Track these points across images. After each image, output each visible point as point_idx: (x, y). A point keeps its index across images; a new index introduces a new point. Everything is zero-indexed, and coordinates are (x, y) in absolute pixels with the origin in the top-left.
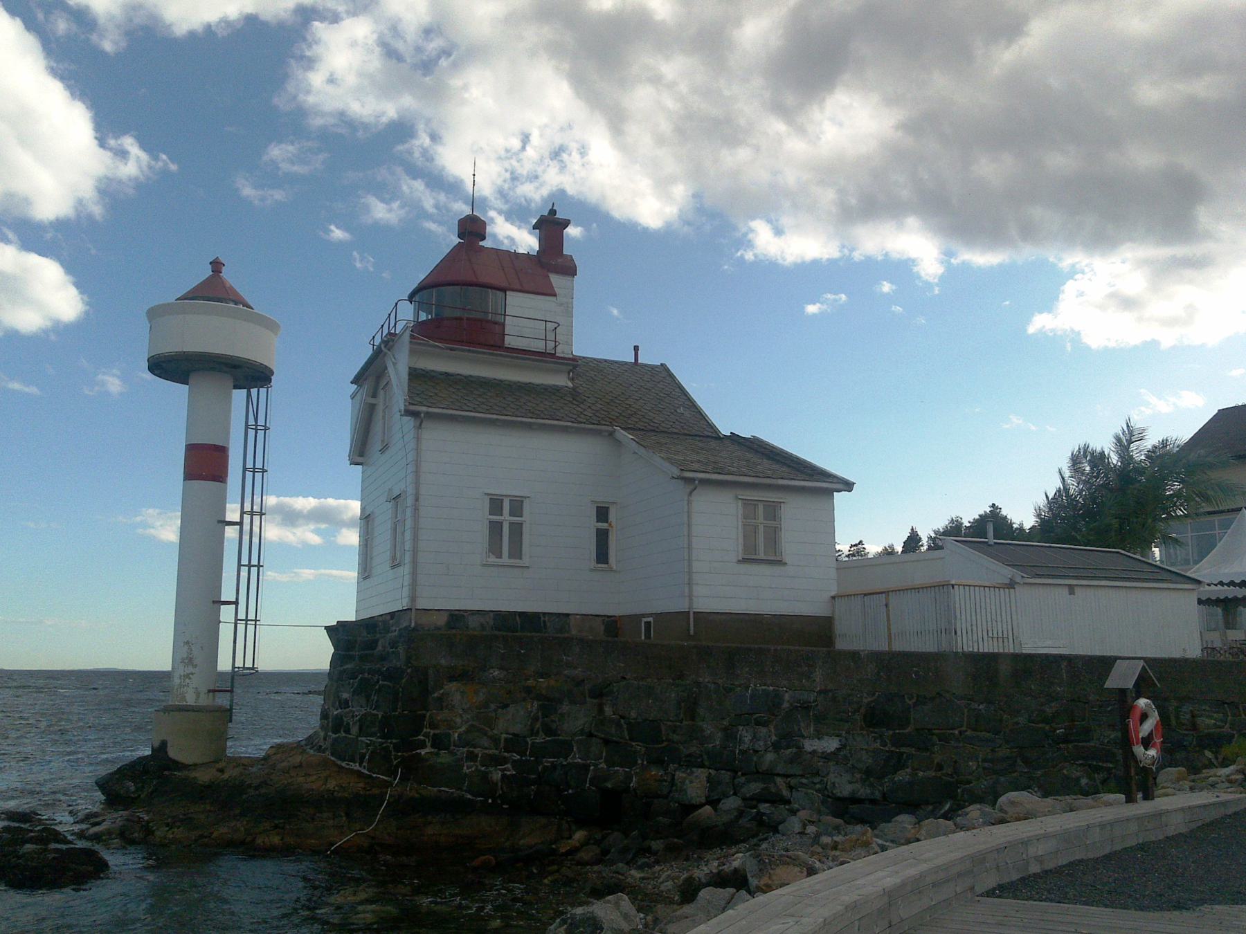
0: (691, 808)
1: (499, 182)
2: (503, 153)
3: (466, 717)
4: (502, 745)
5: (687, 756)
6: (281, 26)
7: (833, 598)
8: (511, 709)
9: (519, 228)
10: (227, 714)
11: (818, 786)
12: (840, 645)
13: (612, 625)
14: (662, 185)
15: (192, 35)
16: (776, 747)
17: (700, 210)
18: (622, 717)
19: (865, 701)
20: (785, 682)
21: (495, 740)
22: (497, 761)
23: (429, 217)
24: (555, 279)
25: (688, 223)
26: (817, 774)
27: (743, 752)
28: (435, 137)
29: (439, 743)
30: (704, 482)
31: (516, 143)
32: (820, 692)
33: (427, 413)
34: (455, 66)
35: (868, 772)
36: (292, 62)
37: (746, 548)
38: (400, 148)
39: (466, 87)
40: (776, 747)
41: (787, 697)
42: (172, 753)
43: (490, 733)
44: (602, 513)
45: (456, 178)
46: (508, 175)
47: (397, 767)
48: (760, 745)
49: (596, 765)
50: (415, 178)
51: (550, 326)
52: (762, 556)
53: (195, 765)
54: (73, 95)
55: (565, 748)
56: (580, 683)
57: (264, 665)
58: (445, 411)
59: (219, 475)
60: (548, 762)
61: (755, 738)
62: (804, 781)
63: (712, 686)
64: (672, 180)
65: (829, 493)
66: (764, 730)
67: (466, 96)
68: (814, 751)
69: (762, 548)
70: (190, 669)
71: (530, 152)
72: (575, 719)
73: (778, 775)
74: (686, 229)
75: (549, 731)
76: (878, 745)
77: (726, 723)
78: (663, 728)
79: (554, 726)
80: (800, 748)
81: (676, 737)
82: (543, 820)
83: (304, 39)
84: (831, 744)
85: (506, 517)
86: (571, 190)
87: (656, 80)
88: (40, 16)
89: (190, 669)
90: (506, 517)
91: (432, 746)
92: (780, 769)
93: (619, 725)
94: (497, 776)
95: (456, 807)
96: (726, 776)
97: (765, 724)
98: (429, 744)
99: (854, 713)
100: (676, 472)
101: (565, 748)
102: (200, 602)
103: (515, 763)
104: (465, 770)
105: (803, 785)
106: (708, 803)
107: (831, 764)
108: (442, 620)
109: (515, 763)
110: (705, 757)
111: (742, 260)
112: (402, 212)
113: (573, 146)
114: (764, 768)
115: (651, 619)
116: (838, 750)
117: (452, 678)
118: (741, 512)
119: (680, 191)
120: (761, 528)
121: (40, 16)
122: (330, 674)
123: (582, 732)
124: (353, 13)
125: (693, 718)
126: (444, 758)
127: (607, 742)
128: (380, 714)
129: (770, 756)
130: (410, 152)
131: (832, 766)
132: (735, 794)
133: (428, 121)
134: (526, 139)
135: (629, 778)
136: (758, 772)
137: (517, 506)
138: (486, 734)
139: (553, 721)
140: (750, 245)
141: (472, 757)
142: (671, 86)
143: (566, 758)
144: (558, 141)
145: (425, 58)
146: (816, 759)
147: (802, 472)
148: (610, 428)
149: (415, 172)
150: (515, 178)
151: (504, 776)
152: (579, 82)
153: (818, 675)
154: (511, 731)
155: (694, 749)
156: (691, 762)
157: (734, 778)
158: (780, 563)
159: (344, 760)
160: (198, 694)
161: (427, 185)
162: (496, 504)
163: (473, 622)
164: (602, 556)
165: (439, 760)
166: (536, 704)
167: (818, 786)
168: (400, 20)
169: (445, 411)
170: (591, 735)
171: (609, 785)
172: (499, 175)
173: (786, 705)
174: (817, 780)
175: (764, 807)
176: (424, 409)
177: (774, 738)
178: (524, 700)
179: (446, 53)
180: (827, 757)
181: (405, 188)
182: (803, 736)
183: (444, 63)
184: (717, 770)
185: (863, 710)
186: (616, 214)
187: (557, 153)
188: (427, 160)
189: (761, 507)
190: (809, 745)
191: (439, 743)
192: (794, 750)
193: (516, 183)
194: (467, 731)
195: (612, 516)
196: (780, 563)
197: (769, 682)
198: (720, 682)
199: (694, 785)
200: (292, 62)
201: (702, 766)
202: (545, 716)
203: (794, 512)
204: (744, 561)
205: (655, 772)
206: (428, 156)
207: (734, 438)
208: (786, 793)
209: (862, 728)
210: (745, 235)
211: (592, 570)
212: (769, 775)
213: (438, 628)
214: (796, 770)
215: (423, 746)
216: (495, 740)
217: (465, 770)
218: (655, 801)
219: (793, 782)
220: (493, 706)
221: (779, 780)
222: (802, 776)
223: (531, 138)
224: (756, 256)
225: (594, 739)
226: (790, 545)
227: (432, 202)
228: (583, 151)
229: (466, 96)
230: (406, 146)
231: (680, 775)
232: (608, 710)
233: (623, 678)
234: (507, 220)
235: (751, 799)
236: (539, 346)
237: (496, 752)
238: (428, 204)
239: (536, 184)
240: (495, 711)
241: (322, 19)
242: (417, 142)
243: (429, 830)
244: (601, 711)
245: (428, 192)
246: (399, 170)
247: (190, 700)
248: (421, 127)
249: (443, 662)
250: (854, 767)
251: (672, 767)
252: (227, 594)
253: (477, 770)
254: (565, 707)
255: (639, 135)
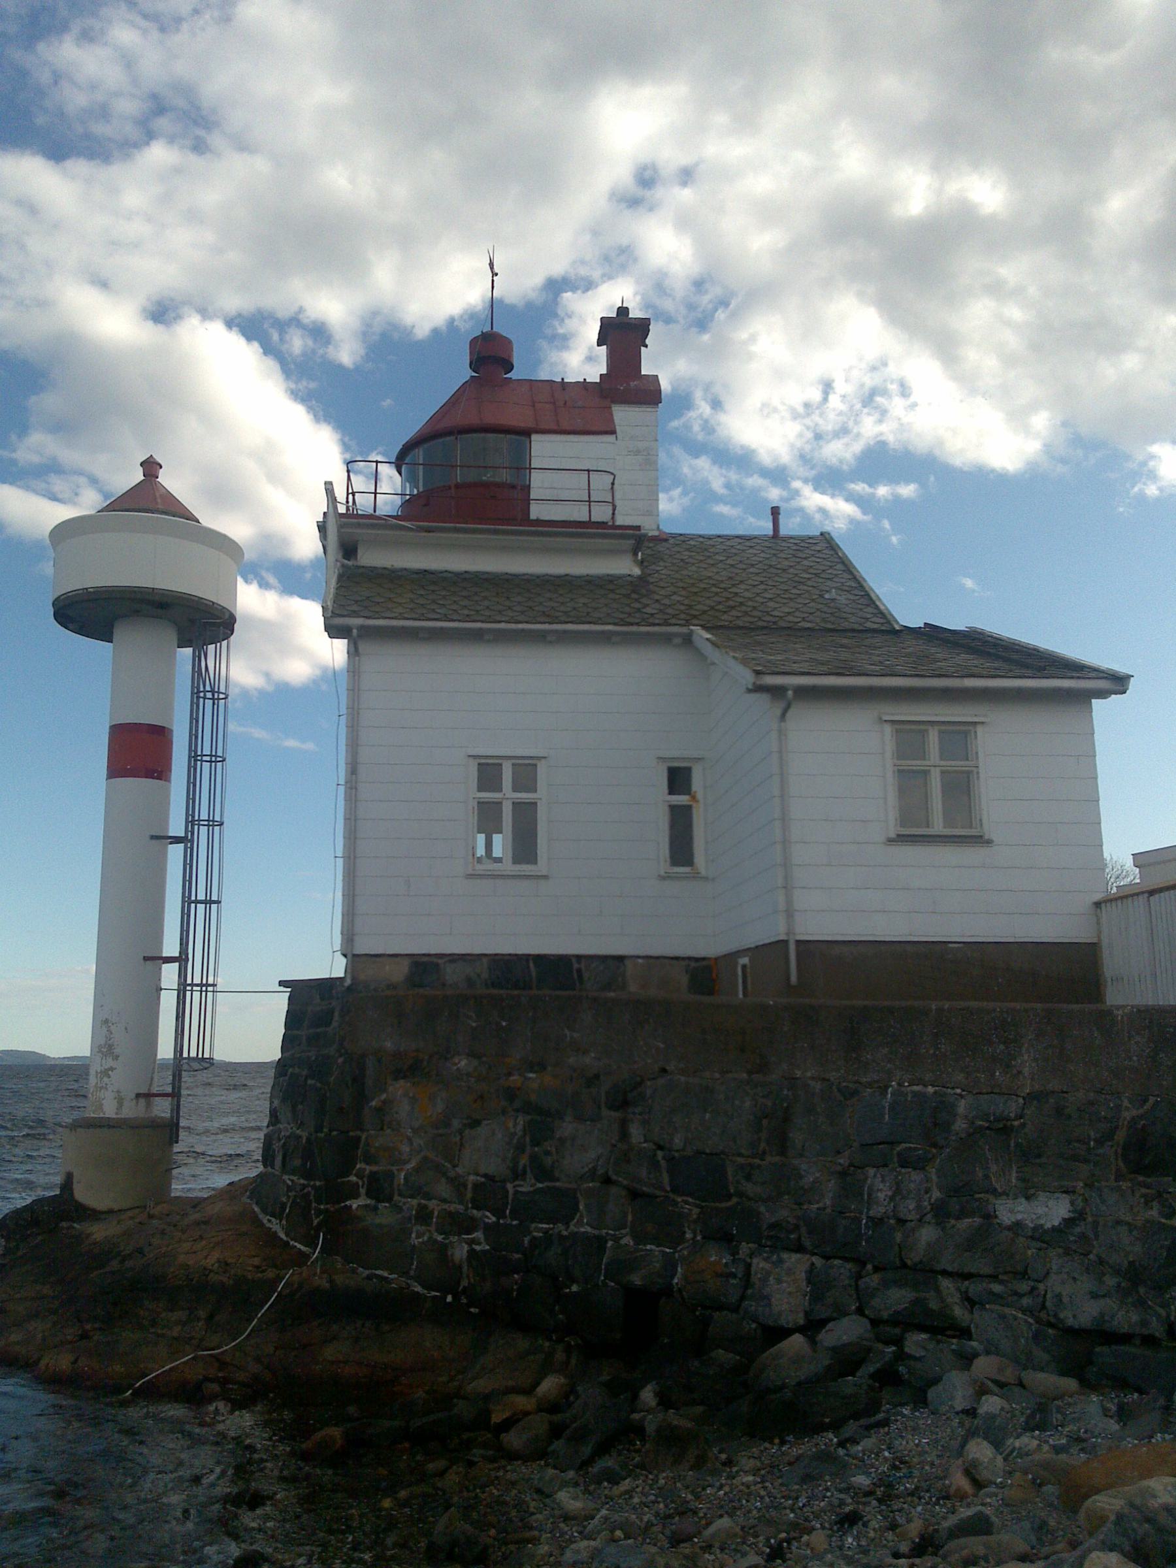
0: (777, 1333)
1: (799, 444)
2: (801, 410)
3: (418, 1142)
4: (469, 1195)
5: (772, 1226)
6: (530, 305)
7: (1098, 905)
8: (483, 1130)
9: (833, 496)
10: (170, 1130)
11: (1025, 1301)
12: (1114, 997)
13: (703, 974)
14: (1018, 417)
15: (436, 331)
16: (941, 1213)
17: (1077, 441)
18: (661, 1148)
19: (1127, 1115)
20: (960, 1077)
21: (458, 1185)
22: (463, 1225)
23: (718, 499)
24: (622, 415)
25: (1063, 461)
26: (1023, 1275)
27: (877, 1222)
28: (716, 404)
29: (379, 1189)
30: (804, 693)
31: (816, 395)
32: (1031, 1097)
33: (361, 628)
34: (733, 315)
35: (1134, 1276)
36: (544, 344)
37: (905, 817)
38: (675, 424)
39: (753, 338)
40: (941, 1213)
41: (962, 1107)
42: (81, 1194)
43: (452, 1174)
44: (678, 779)
45: (742, 447)
46: (809, 435)
47: (318, 1229)
48: (908, 1209)
49: (617, 1240)
50: (697, 457)
51: (600, 483)
52: (938, 826)
53: (111, 1212)
54: (317, 419)
55: (563, 1205)
56: (593, 1080)
57: (218, 1056)
58: (394, 623)
59: (158, 770)
60: (539, 1229)
61: (898, 1192)
62: (997, 1288)
63: (817, 1086)
64: (1033, 407)
65: (1083, 698)
66: (916, 1176)
67: (753, 348)
68: (1018, 1225)
69: (940, 812)
70: (110, 1063)
71: (834, 401)
72: (582, 1149)
73: (945, 1273)
74: (1061, 469)
75: (543, 1173)
76: (1154, 1213)
77: (843, 1160)
78: (730, 1171)
79: (548, 1161)
80: (989, 1217)
81: (749, 1188)
82: (523, 1343)
83: (556, 315)
84: (1053, 1210)
85: (508, 794)
86: (890, 438)
87: (996, 289)
88: (276, 337)
89: (110, 1063)
90: (508, 794)
91: (369, 1195)
92: (946, 1262)
93: (655, 1165)
94: (460, 1252)
95: (387, 1309)
96: (842, 1270)
97: (919, 1164)
98: (363, 1191)
99: (1100, 1142)
100: (748, 678)
101: (563, 1205)
102: (138, 961)
103: (488, 1228)
104: (415, 1240)
105: (997, 1298)
106: (800, 1330)
107: (1052, 1253)
108: (399, 973)
109: (488, 1228)
110: (803, 1230)
111: (1142, 498)
112: (686, 501)
113: (893, 387)
114: (913, 1258)
115: (745, 960)
116: (1069, 1222)
117: (398, 1074)
118: (890, 747)
119: (1041, 421)
120: (935, 775)
121: (276, 337)
122: (281, 1065)
123: (592, 1174)
124: (608, 277)
125: (783, 1152)
126: (385, 1217)
127: (634, 1195)
128: (305, 1135)
129: (927, 1234)
130: (688, 427)
131: (1055, 1257)
132: (860, 1311)
133: (707, 387)
134: (827, 387)
135: (670, 1265)
136: (904, 1266)
137: (526, 772)
138: (444, 1174)
139: (548, 1153)
140: (1153, 476)
141: (423, 1216)
142: (1017, 293)
143: (567, 1224)
144: (869, 381)
145: (700, 315)
146: (1021, 1241)
147: (1027, 667)
148: (684, 630)
149: (696, 449)
150: (818, 437)
151: (472, 1253)
152: (895, 312)
153: (1026, 1062)
154: (483, 1170)
155: (784, 1213)
156: (780, 1240)
157: (859, 1277)
158: (980, 840)
159: (266, 1213)
160: (120, 1101)
161: (714, 462)
162: (488, 773)
163: (453, 975)
164: (681, 848)
165: (378, 1221)
166: (521, 1121)
167: (1025, 1301)
168: (666, 275)
169: (394, 623)
170: (607, 1181)
171: (636, 1279)
172: (800, 435)
173: (960, 1125)
174: (1024, 1287)
175: (915, 1342)
176: (359, 621)
177: (936, 1194)
178: (504, 1112)
179: (724, 303)
180: (1044, 1237)
181: (686, 470)
182: (994, 1192)
183: (721, 315)
184: (827, 1258)
185: (1121, 1136)
186: (957, 462)
187: (870, 398)
188: (709, 434)
189: (933, 736)
190: (1010, 1211)
191: (379, 1189)
192: (978, 1220)
193: (821, 443)
194: (418, 1170)
195: (697, 782)
196: (980, 840)
197: (928, 1077)
198: (833, 1076)
199: (784, 1286)
200: (544, 344)
201: (799, 1248)
202: (536, 1143)
203: (1007, 746)
204: (902, 839)
205: (716, 1257)
206: (709, 428)
207: (932, 633)
208: (959, 1312)
209: (1119, 1177)
210: (1144, 464)
211: (663, 878)
212: (925, 1273)
213: (392, 986)
214: (981, 1265)
215: (356, 1196)
216: (458, 1185)
217: (415, 1240)
218: (716, 1315)
219: (975, 1288)
220: (456, 1124)
221: (946, 1284)
222: (994, 1277)
223: (835, 385)
224: (1161, 489)
225: (614, 1190)
226: (995, 804)
227: (721, 481)
228: (904, 390)
229: (753, 348)
230: (683, 420)
231: (759, 1264)
232: (636, 1133)
233: (664, 1070)
234: (816, 489)
235: (894, 1321)
236: (579, 513)
237: (461, 1208)
238: (717, 485)
239: (845, 440)
240: (461, 1132)
241: (574, 289)
242: (692, 414)
243: (330, 1352)
244: (624, 1135)
245: (716, 469)
246: (677, 450)
247: (109, 1110)
248: (698, 394)
249: (388, 1044)
250: (1101, 1261)
251: (745, 1248)
252: (171, 948)
253: (430, 1238)
254: (567, 1127)
255: (982, 360)
